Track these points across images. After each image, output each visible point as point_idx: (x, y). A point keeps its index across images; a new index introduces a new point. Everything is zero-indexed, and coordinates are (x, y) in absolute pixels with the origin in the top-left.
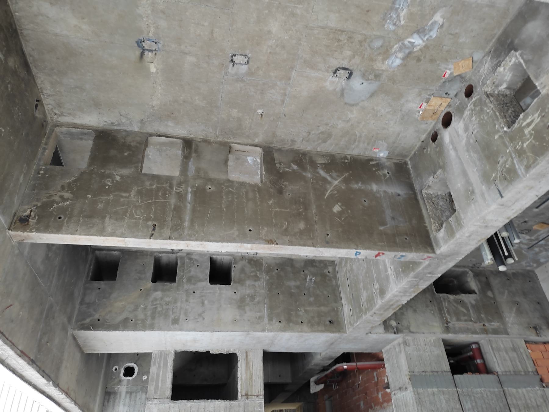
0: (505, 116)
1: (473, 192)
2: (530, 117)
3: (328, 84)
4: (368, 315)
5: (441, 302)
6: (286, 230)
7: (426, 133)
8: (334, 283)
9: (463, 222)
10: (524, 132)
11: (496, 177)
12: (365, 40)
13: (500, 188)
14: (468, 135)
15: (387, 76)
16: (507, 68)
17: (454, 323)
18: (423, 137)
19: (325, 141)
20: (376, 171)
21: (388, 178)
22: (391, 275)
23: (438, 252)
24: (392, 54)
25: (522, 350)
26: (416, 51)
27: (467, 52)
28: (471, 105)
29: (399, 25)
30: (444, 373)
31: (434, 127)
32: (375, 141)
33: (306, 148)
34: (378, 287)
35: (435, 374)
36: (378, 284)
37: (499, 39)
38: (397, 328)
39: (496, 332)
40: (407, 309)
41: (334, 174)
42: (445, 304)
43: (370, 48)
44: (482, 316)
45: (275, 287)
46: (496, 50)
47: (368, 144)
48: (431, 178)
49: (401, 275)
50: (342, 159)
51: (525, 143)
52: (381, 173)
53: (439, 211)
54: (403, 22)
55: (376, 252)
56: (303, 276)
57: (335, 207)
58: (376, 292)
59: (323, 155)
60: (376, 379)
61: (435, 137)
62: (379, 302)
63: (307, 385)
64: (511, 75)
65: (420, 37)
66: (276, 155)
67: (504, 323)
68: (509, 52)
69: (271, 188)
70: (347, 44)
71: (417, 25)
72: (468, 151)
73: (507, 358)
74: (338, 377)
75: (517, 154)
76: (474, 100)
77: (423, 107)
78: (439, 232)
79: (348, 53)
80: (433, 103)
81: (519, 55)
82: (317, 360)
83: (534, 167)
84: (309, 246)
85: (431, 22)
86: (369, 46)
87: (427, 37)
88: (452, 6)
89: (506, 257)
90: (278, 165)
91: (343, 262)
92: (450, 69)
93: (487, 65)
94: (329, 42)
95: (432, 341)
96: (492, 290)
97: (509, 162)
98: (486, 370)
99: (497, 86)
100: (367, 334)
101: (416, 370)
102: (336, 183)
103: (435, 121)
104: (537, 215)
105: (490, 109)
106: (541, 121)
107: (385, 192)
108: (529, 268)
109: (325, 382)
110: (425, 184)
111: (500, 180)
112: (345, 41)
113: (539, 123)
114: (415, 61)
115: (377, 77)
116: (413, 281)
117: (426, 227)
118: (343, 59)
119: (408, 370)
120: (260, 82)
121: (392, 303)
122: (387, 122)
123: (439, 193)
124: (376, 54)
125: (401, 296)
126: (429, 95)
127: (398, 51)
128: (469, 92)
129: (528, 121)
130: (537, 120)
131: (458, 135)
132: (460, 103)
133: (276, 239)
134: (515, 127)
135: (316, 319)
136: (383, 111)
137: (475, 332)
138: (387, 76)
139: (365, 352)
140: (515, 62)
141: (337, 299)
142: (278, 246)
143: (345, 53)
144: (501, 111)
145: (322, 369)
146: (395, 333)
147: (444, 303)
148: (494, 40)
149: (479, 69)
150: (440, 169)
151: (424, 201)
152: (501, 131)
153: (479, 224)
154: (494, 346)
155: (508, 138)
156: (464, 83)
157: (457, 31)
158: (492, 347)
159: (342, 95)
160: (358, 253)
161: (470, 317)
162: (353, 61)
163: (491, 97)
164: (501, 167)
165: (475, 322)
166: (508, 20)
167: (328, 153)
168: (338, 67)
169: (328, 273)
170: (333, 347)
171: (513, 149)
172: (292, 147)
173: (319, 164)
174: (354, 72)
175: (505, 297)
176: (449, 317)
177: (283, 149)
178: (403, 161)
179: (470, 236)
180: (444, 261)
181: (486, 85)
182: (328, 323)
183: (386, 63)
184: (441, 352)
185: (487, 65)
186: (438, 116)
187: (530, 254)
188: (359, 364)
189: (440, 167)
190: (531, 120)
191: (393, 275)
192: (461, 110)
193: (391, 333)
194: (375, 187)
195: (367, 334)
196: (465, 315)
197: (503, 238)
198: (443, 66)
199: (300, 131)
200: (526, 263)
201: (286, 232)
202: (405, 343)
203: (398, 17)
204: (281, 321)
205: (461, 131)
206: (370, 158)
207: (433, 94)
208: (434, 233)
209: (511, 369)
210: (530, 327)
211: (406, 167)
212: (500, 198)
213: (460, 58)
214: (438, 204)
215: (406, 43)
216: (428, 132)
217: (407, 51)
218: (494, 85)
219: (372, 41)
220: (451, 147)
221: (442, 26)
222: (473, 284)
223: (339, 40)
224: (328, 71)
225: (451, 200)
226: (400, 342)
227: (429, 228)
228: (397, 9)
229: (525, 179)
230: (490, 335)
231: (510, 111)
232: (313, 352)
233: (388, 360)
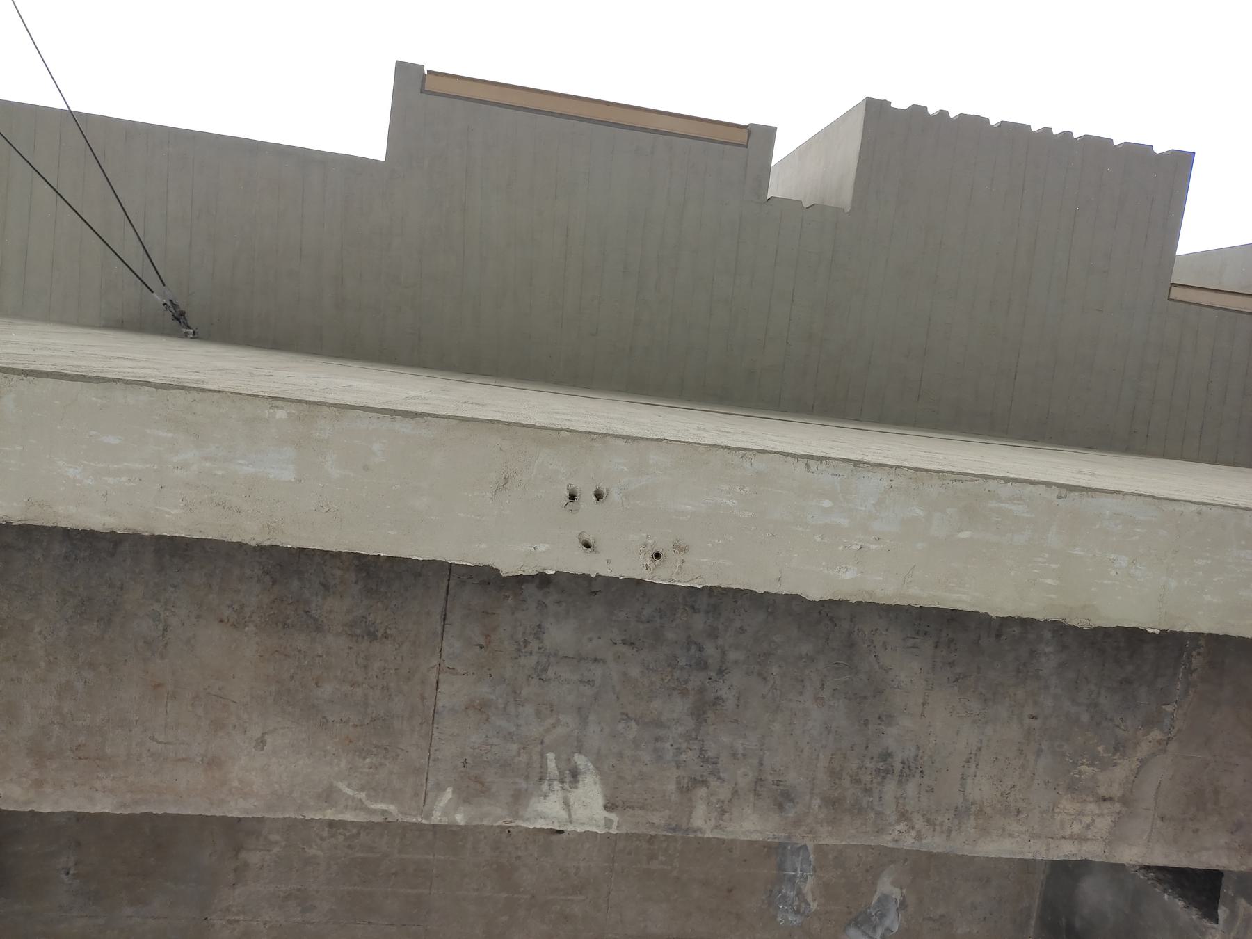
85: (875, 899)
88: (906, 860)
148: (1033, 922)
221: (903, 905)
228: (792, 880)
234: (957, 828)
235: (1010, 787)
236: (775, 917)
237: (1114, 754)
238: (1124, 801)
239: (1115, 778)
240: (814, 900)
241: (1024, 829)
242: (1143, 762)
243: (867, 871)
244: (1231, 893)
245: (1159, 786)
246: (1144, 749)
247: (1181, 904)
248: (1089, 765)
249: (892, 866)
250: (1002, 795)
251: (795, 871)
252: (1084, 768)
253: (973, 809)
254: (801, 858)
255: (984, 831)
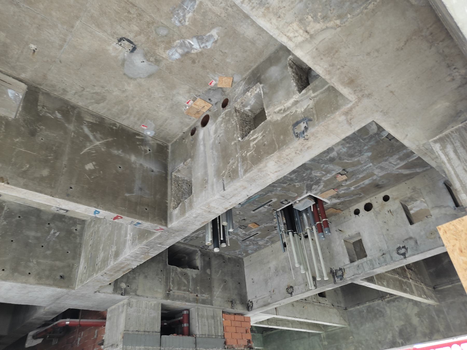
0: (243, 130)
1: (207, 182)
2: (256, 134)
3: (110, 48)
4: (99, 274)
5: (170, 272)
6: (25, 172)
7: (188, 127)
8: (78, 241)
9: (194, 205)
10: (250, 144)
11: (224, 173)
12: (153, 23)
13: (225, 183)
14: (215, 136)
15: (166, 65)
16: (253, 95)
17: (175, 292)
18: (186, 129)
19: (98, 102)
20: (139, 145)
21: (148, 154)
22: (129, 240)
23: (169, 226)
24: (173, 47)
25: (218, 319)
26: (193, 53)
27: (230, 71)
28: (223, 114)
29: (183, 24)
30: (154, 333)
31: (195, 124)
32: (145, 119)
33: (78, 103)
34: (115, 250)
35: (147, 333)
36: (116, 247)
37: (253, 71)
38: (125, 290)
39: (204, 302)
40: (139, 275)
41: (98, 136)
42: (172, 275)
43: (156, 32)
44: (198, 288)
45: (10, 234)
46: (249, 79)
47: (138, 119)
48: (182, 164)
49: (137, 241)
50: (111, 124)
51: (249, 153)
52: (143, 148)
53: (180, 193)
54: (187, 23)
55: (115, 215)
56: (47, 229)
57: (88, 165)
58: (112, 254)
59: (93, 115)
60: (95, 336)
61: (193, 132)
62: (112, 263)
63: (24, 339)
64: (254, 101)
65: (198, 42)
66: (41, 98)
67: (212, 296)
68: (256, 83)
69: (23, 127)
70: (135, 20)
71: (198, 31)
72: (212, 149)
73: (207, 324)
74: (61, 333)
75: (242, 160)
76: (226, 111)
77: (190, 103)
78: (175, 210)
79: (136, 28)
80: (198, 103)
81: (262, 87)
82: (40, 314)
83: (250, 172)
84: (46, 194)
85: (208, 34)
86: (155, 30)
87: (203, 45)
88: (226, 29)
89: (222, 242)
90: (40, 108)
91: (93, 223)
92: (215, 80)
93: (241, 88)
94: (119, 9)
95: (153, 305)
96: (210, 269)
97: (235, 165)
98: (189, 333)
99: (244, 106)
100: (95, 292)
101: (131, 329)
102: (98, 143)
103: (197, 119)
104: (253, 216)
105: (235, 121)
106: (262, 139)
107: (141, 165)
108: (240, 256)
109: (44, 337)
110: (176, 167)
111: (226, 177)
112: (135, 16)
113: (260, 140)
114: (191, 61)
115: (157, 61)
116: (144, 248)
117: (167, 203)
118: (129, 32)
119: (124, 329)
120: (39, 16)
121: (123, 266)
122: (158, 105)
123: (186, 179)
124: (160, 40)
125: (132, 261)
126: (196, 95)
127: (179, 46)
128: (225, 105)
129: (255, 137)
130: (260, 138)
131: (209, 135)
132: (217, 111)
133: (8, 179)
134: (246, 139)
135: (47, 273)
136: (156, 94)
137: (188, 301)
138: (166, 65)
139: (91, 309)
140: (258, 92)
141: (76, 255)
142: (9, 186)
143: (132, 26)
144: (241, 125)
145: (43, 323)
146: (122, 295)
147: (171, 274)
148: (250, 71)
149: (235, 89)
150: (191, 158)
151: (172, 182)
152: (237, 140)
153: (204, 208)
154: (200, 314)
155: (239, 146)
156: (224, 96)
157: (226, 51)
158: (198, 314)
159: (123, 65)
160: (97, 212)
161: (189, 288)
162: (139, 38)
163: (237, 112)
164: (229, 166)
165: (191, 293)
166: (262, 60)
167: (99, 115)
168: (124, 37)
169: (75, 231)
170: (58, 301)
171: (240, 155)
172: (62, 96)
173: (86, 121)
174: (137, 48)
175: (218, 276)
176: (173, 286)
177: (52, 95)
178: (166, 145)
179: (196, 217)
180: (173, 235)
181: (236, 102)
182: (58, 277)
183: (167, 53)
184: (158, 315)
185: (241, 88)
186: (200, 115)
187: (243, 245)
188: (82, 320)
189: (191, 157)
190: (256, 136)
191: (130, 240)
192: (216, 115)
193: (119, 294)
194: (133, 158)
195: (95, 292)
196: (185, 285)
197: (223, 226)
198: (211, 75)
199: (74, 83)
200: (239, 252)
201: (24, 174)
202: (129, 304)
203: (184, 16)
204: (5, 270)
205: (212, 132)
206: (138, 132)
207: (199, 96)
208: (171, 209)
209: (207, 333)
210: (229, 301)
211: (166, 151)
212: (223, 190)
213: (224, 74)
214: (182, 187)
215: (186, 42)
216: (190, 126)
217: (186, 50)
218: (242, 104)
219: (158, 27)
220: (202, 143)
221: (216, 42)
222: (198, 262)
223: (129, 12)
224: (113, 36)
225: (190, 185)
226: (125, 303)
227: (168, 205)
228: (184, 9)
229: (242, 179)
230: (199, 304)
231: (247, 128)
232: (36, 305)
233: (110, 318)
234: (257, 8)
235: (283, 6)
236: (171, 18)
237: (321, 19)
238: (312, 37)
239: (314, 27)
240: (188, 22)
241: (277, 24)
242: (327, 28)
243: (211, 24)
244: (310, 88)
245: (324, 39)
246: (331, 24)
247: (295, 84)
248: (312, 17)
249: (221, 27)
250: (279, 7)
251: (187, 7)
252: (310, 17)
253: (267, 5)
254: (192, 4)
255: (264, 15)
